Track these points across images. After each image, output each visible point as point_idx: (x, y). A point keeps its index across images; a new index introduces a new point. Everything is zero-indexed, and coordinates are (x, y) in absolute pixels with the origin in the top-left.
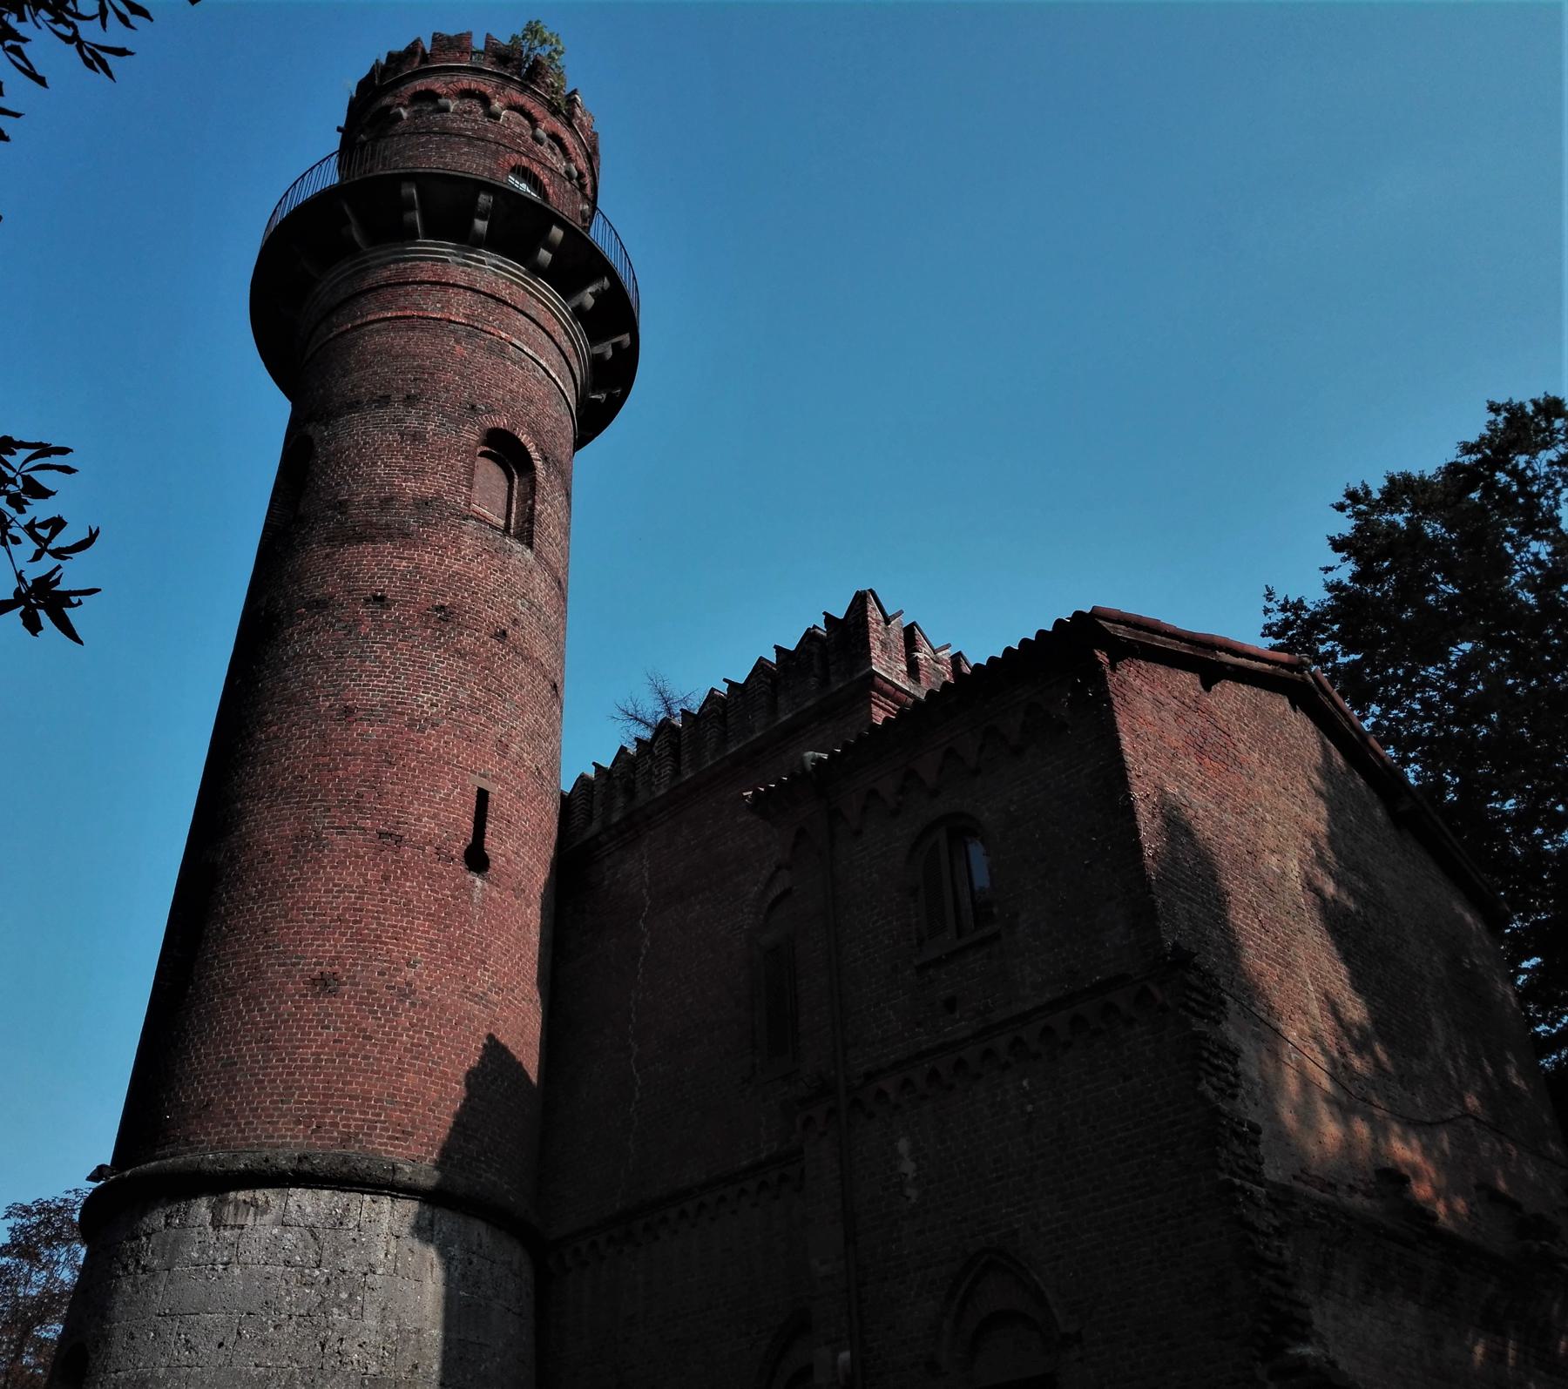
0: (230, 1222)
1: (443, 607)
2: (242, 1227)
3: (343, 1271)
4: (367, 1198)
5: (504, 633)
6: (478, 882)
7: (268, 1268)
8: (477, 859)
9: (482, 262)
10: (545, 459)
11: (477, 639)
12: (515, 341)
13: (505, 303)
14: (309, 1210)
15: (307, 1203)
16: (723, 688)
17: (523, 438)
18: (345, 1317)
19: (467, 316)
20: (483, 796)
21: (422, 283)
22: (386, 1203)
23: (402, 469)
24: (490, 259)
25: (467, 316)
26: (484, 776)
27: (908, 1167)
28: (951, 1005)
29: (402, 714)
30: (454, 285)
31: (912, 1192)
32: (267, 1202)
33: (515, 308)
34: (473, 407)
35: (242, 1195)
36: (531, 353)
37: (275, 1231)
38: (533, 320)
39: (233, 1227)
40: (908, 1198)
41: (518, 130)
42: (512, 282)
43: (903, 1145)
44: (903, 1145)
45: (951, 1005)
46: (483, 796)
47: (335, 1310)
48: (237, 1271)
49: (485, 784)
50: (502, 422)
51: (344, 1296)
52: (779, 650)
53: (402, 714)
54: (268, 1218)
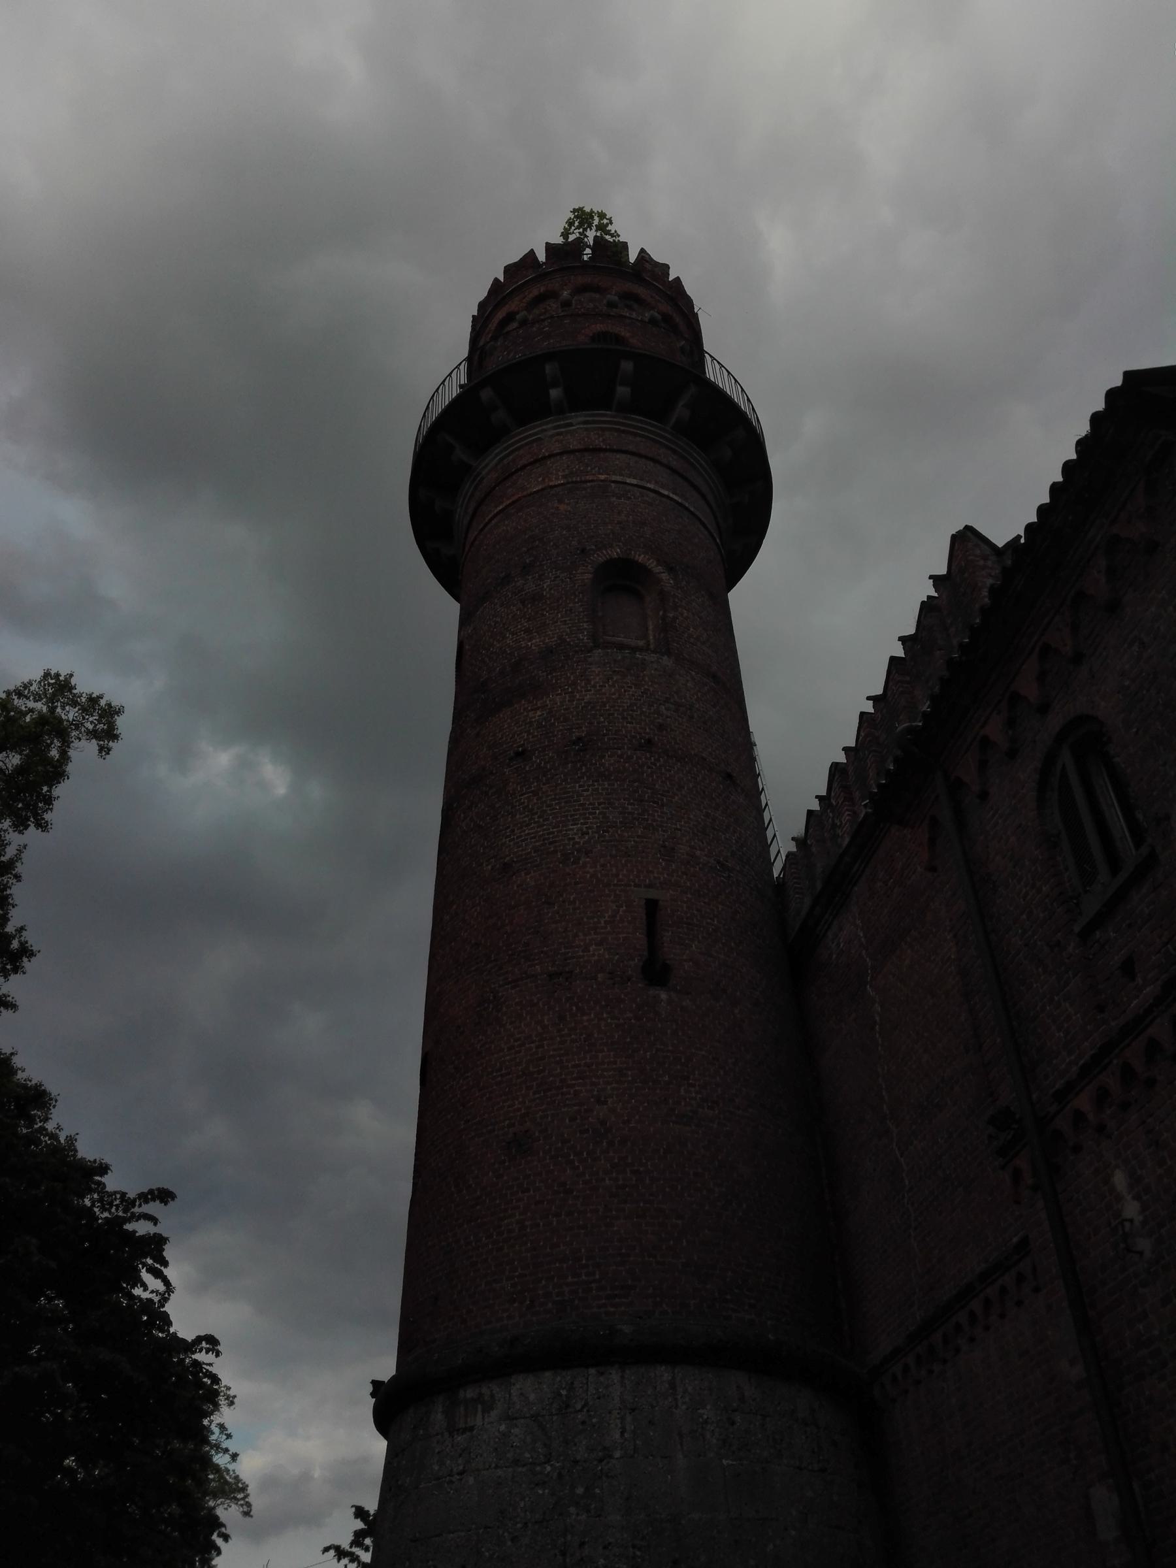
0: (462, 1425)
1: (579, 739)
2: (472, 1429)
3: (576, 1462)
4: (592, 1371)
5: (649, 741)
6: (664, 996)
7: (499, 1472)
8: (656, 972)
9: (571, 425)
10: (671, 570)
11: (621, 756)
12: (614, 478)
13: (600, 450)
14: (532, 1397)
15: (529, 1390)
16: (869, 707)
17: (641, 559)
18: (584, 1517)
19: (564, 477)
20: (652, 907)
21: (524, 467)
22: (614, 1375)
23: (528, 631)
24: (577, 419)
25: (564, 477)
26: (650, 886)
27: (1131, 1209)
28: (1128, 968)
29: (555, 852)
30: (550, 456)
31: (1144, 1245)
32: (492, 1396)
33: (612, 451)
34: (583, 551)
35: (469, 1393)
36: (634, 482)
37: (503, 1428)
38: (633, 454)
39: (465, 1430)
40: (1141, 1253)
41: (591, 305)
42: (603, 429)
43: (1119, 1179)
44: (1119, 1179)
45: (1128, 968)
46: (652, 907)
47: (572, 1510)
48: (471, 1480)
49: (653, 894)
50: (615, 552)
51: (580, 1491)
52: (902, 639)
53: (555, 852)
54: (494, 1414)
